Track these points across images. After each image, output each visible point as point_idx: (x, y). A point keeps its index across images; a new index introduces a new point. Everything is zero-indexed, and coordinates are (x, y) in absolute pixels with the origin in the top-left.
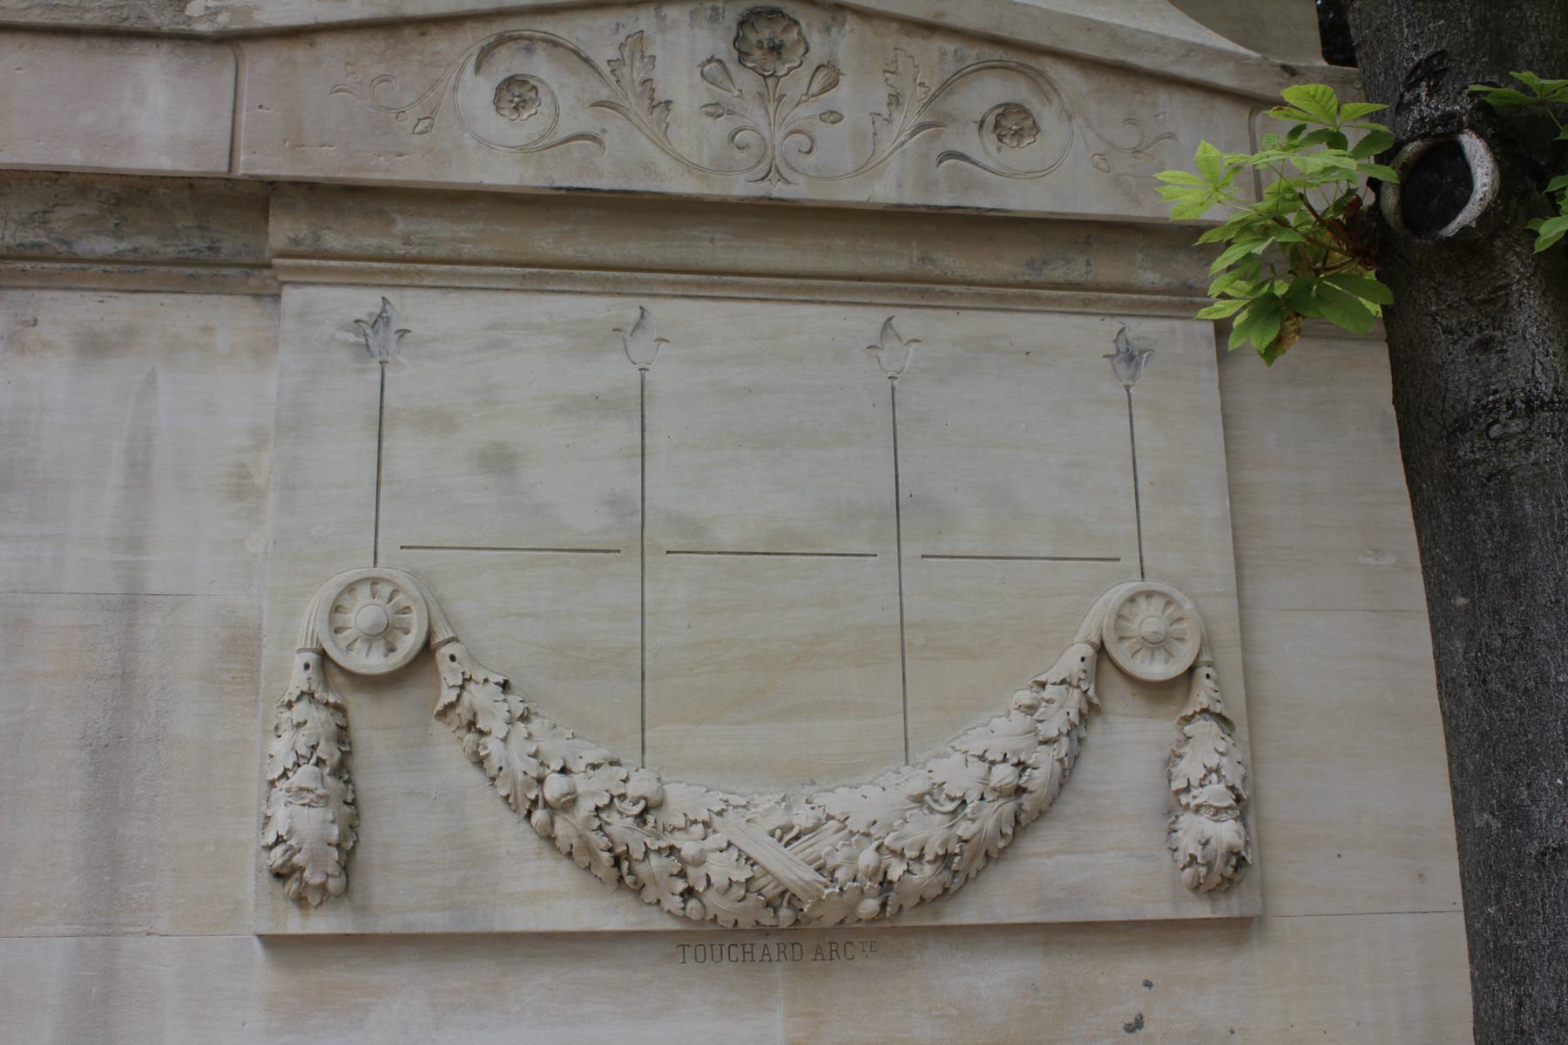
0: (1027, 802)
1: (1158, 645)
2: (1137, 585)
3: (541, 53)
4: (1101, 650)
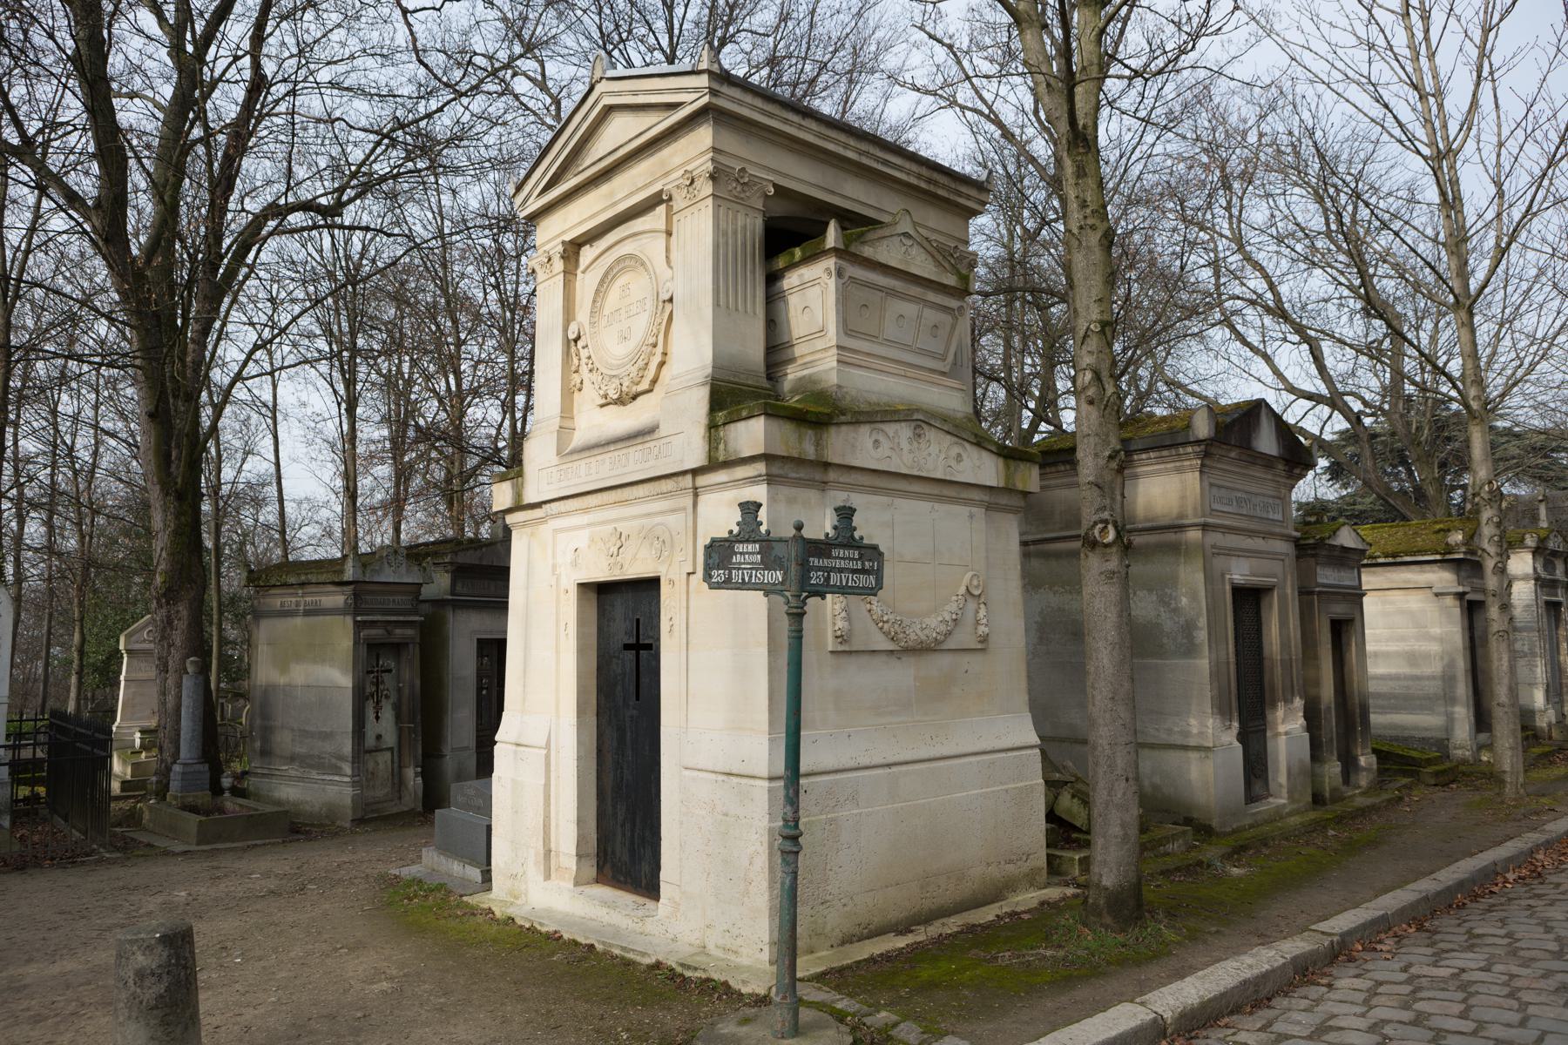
1: (977, 587)
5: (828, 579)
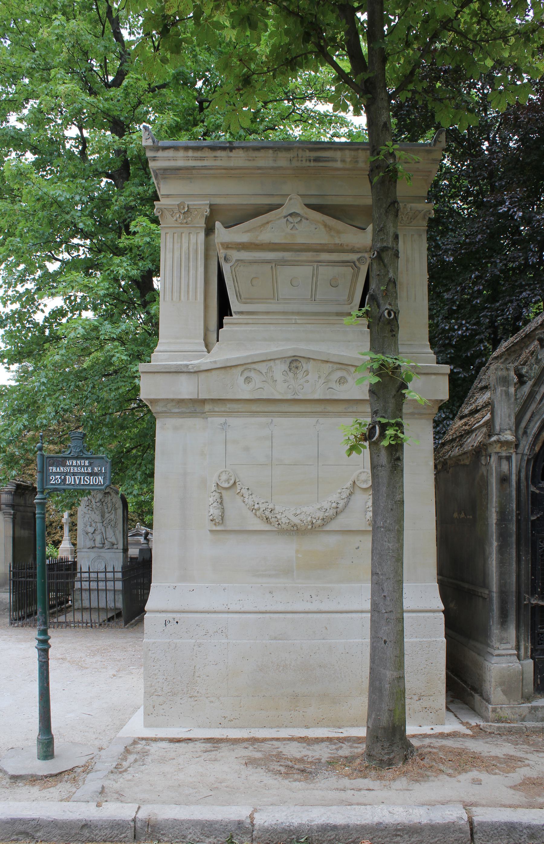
0: (338, 510)
2: (363, 470)
3: (253, 371)
4: (354, 482)
5: (65, 479)
